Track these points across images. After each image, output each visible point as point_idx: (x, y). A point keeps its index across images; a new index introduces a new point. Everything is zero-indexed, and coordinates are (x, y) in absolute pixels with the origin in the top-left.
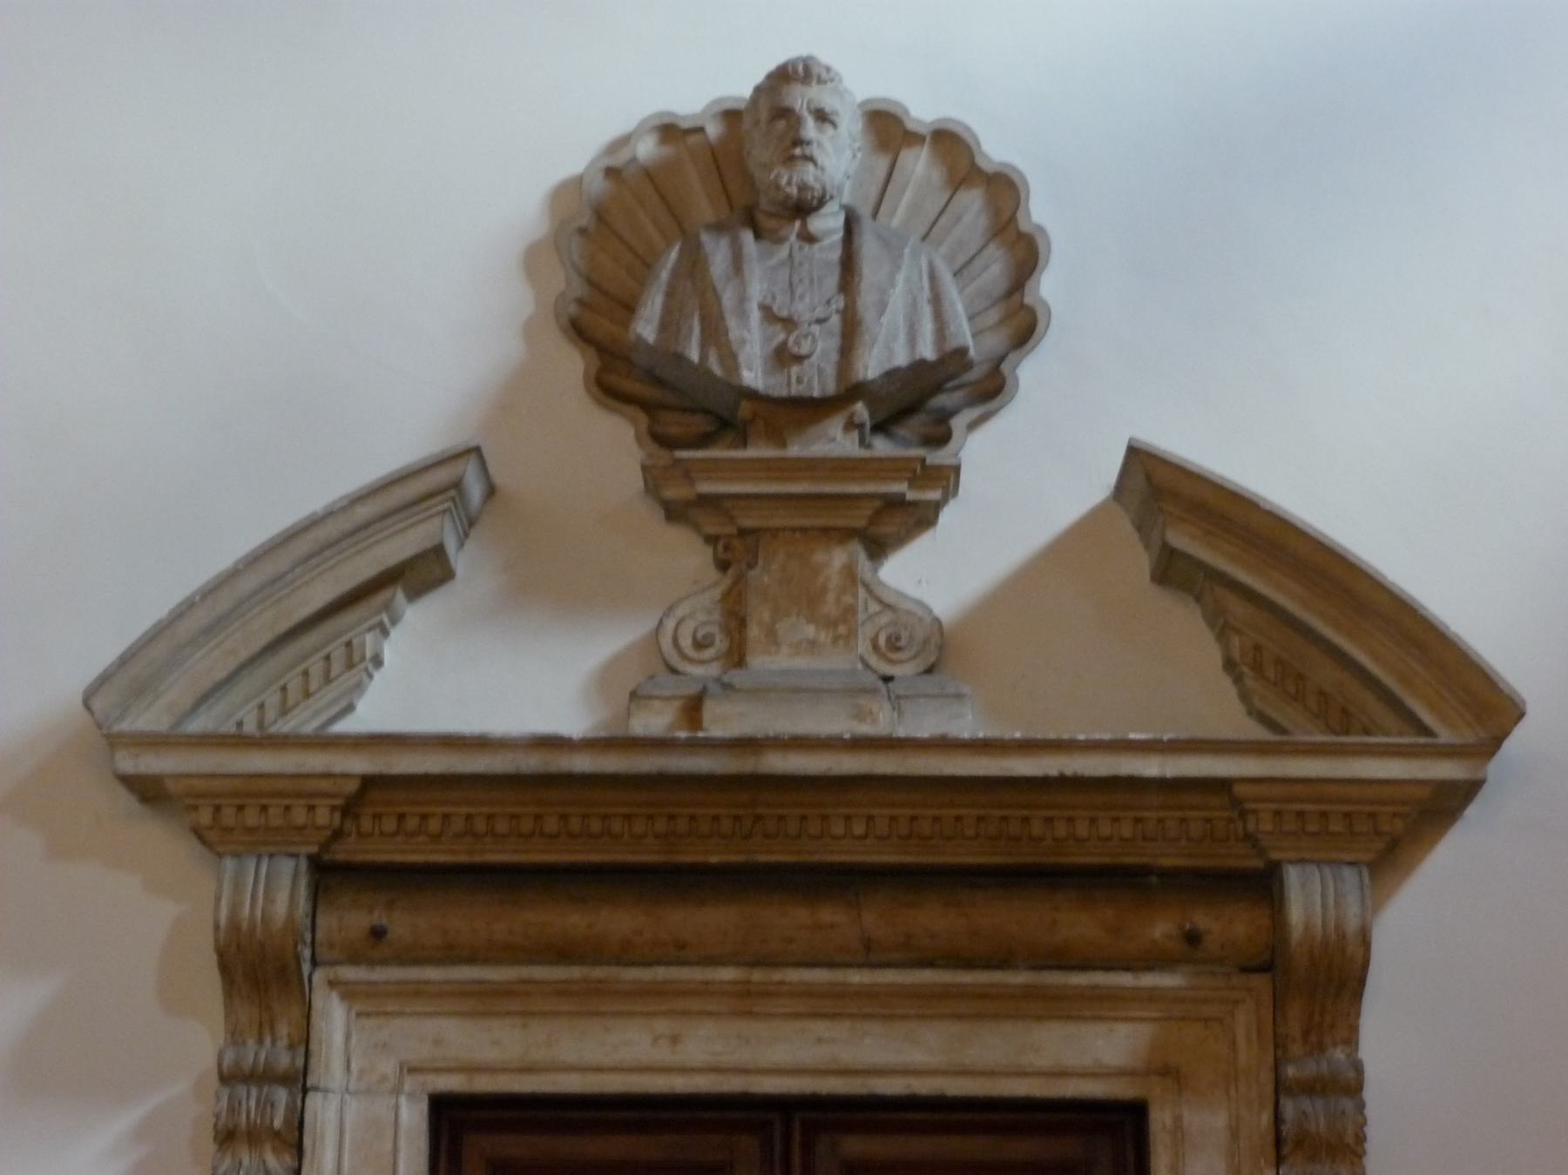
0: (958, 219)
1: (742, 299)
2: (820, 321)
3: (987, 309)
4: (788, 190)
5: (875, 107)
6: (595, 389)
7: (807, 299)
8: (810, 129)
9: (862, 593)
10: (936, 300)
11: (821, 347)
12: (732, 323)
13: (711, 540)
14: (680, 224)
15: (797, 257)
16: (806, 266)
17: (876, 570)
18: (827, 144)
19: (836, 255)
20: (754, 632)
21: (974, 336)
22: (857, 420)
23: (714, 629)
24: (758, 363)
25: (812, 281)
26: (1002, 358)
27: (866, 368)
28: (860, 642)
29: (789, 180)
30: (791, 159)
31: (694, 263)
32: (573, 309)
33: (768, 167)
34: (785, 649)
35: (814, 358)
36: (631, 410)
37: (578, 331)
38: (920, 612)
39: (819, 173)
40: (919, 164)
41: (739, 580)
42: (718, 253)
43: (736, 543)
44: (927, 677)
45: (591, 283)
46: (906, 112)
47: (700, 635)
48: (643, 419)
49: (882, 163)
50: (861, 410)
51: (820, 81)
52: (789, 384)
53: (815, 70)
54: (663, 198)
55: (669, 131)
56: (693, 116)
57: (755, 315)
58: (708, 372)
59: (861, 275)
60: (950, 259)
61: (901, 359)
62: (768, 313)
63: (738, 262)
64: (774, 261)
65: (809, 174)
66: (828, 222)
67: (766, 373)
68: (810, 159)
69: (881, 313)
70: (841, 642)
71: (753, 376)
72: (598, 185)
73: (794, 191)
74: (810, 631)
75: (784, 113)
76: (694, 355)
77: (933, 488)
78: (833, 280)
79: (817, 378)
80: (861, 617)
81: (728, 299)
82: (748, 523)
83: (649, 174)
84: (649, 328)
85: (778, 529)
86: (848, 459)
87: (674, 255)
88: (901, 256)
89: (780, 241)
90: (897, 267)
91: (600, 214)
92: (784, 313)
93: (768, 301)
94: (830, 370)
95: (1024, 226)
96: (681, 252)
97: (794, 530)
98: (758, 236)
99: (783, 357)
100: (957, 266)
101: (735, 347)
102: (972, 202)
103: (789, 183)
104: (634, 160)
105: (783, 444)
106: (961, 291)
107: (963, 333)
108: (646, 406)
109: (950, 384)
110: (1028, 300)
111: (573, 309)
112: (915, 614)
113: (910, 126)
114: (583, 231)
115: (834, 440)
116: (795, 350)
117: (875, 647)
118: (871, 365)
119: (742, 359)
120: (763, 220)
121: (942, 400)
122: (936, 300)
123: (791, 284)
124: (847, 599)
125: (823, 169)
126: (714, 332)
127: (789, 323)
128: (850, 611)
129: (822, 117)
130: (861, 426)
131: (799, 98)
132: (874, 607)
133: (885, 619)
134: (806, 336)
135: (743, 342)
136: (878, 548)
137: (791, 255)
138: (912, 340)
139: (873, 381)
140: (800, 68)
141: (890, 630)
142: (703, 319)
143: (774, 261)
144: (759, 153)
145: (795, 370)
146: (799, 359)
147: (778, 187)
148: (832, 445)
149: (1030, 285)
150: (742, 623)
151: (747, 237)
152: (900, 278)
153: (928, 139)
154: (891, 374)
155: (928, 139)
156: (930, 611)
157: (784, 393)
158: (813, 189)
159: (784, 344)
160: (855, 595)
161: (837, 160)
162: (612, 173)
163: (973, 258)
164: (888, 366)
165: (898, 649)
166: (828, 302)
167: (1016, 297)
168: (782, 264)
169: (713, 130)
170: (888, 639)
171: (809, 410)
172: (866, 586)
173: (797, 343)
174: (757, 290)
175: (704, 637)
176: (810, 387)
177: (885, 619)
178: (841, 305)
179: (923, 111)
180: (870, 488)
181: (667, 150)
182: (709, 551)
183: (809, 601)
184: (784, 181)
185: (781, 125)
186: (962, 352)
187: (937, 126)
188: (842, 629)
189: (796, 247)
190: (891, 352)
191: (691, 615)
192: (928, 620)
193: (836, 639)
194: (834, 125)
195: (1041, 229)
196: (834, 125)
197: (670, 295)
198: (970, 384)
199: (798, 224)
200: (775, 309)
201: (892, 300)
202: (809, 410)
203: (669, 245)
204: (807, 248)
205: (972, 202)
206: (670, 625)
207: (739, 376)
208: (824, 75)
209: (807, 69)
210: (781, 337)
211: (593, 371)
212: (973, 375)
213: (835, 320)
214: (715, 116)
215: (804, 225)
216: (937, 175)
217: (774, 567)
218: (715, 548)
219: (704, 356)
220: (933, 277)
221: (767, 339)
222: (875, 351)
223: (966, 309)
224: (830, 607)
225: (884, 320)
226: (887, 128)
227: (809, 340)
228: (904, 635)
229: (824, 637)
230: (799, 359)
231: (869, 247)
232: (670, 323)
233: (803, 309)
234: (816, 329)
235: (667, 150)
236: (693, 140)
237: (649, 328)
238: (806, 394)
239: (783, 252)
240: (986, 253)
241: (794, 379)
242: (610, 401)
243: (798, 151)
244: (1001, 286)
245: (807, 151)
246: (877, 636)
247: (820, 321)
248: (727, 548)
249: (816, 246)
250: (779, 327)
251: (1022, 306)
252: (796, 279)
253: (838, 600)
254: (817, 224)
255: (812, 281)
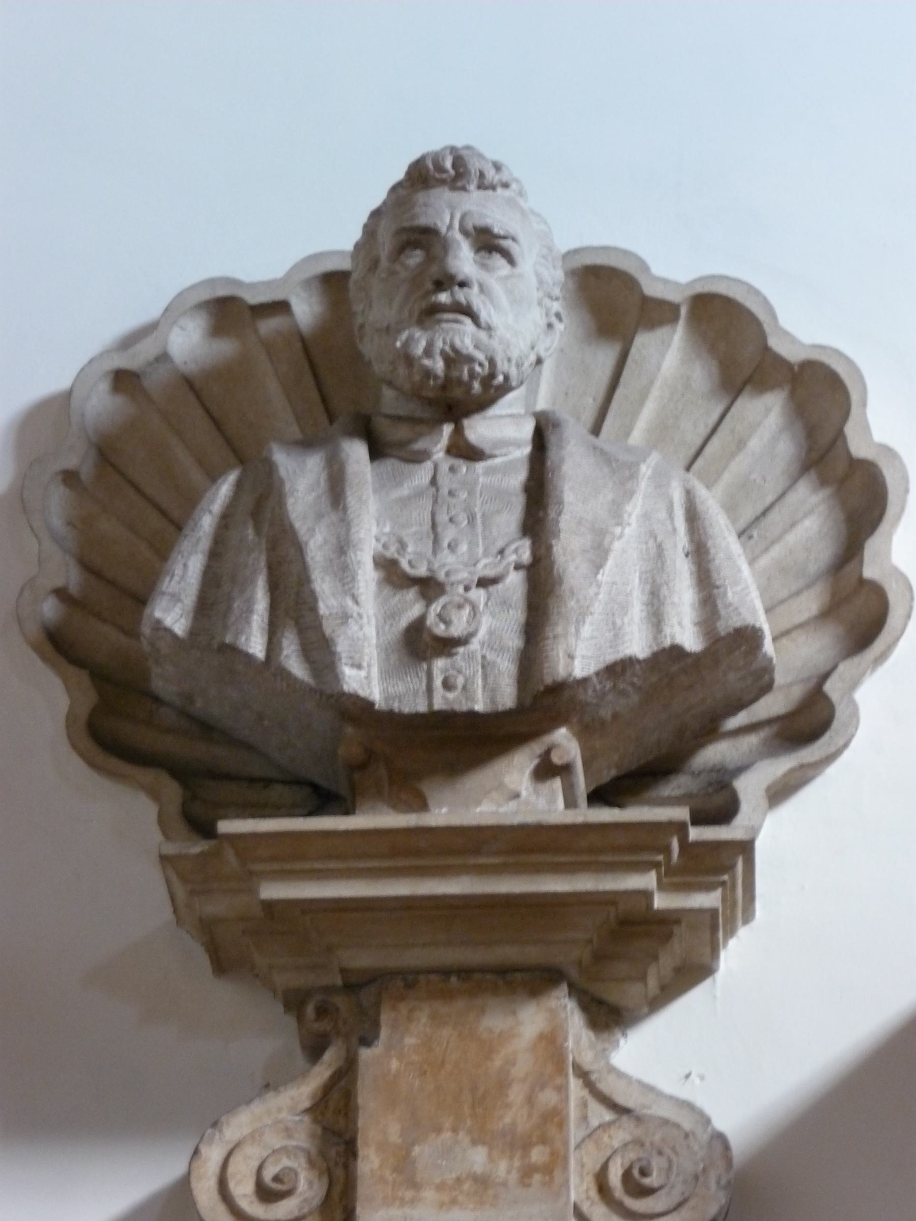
0: (741, 444)
1: (343, 547)
2: (484, 583)
3: (798, 593)
4: (427, 362)
5: (589, 260)
6: (87, 743)
7: (463, 548)
8: (464, 260)
9: (574, 1085)
10: (700, 553)
11: (490, 628)
12: (323, 585)
13: (294, 1002)
14: (234, 451)
15: (445, 481)
16: (463, 495)
17: (604, 1054)
18: (497, 288)
19: (518, 478)
20: (369, 1162)
21: (768, 611)
22: (556, 759)
23: (299, 1164)
24: (371, 654)
25: (472, 519)
26: (825, 676)
27: (571, 657)
28: (573, 1180)
29: (427, 346)
30: (430, 314)
31: (262, 501)
32: (50, 609)
33: (390, 331)
34: (429, 1194)
35: (475, 645)
36: (148, 775)
37: (59, 645)
38: (687, 1124)
39: (483, 335)
40: (668, 358)
41: (346, 1073)
42: (301, 479)
43: (340, 1002)
44: (687, 1072)
45: (86, 566)
46: (644, 266)
47: (269, 1174)
48: (173, 790)
49: (603, 358)
50: (565, 742)
51: (483, 185)
52: (430, 690)
53: (474, 165)
54: (217, 423)
55: (227, 311)
56: (269, 284)
57: (367, 577)
58: (284, 674)
59: (561, 503)
60: (731, 508)
61: (637, 644)
62: (392, 573)
63: (336, 488)
64: (405, 490)
65: (464, 336)
66: (503, 428)
67: (387, 674)
68: (468, 311)
69: (598, 566)
70: (537, 1178)
71: (367, 674)
72: (100, 403)
73: (438, 365)
74: (478, 1158)
75: (424, 239)
76: (256, 646)
77: (709, 888)
78: (509, 519)
79: (482, 680)
80: (575, 1133)
81: (317, 546)
82: (362, 959)
83: (191, 385)
84: (178, 610)
85: (418, 972)
86: (540, 829)
87: (225, 489)
88: (633, 476)
89: (419, 458)
90: (629, 495)
91: (107, 452)
92: (422, 571)
93: (392, 552)
94: (506, 668)
95: (858, 448)
96: (239, 485)
97: (446, 972)
98: (376, 453)
99: (420, 645)
100: (742, 523)
101: (328, 628)
102: (765, 418)
103: (428, 352)
104: (164, 357)
105: (422, 805)
106: (752, 562)
107: (748, 599)
108: (180, 772)
109: (733, 723)
110: (869, 572)
111: (50, 609)
112: (677, 1126)
113: (651, 290)
114: (70, 477)
115: (511, 793)
116: (440, 630)
117: (603, 1188)
118: (580, 653)
119: (342, 647)
120: (383, 426)
121: (715, 753)
122: (700, 553)
123: (434, 526)
124: (548, 1098)
125: (489, 329)
126: (293, 605)
127: (429, 587)
128: (555, 1118)
129: (488, 243)
130: (565, 770)
131: (444, 211)
132: (600, 1115)
133: (620, 1136)
134: (460, 607)
135: (345, 617)
136: (608, 1017)
137: (434, 482)
138: (656, 616)
139: (584, 682)
140: (448, 164)
141: (632, 1155)
142: (274, 588)
143: (405, 490)
144: (377, 310)
145: (440, 664)
146: (447, 646)
147: (409, 360)
148: (512, 805)
149: (872, 546)
150: (350, 1149)
151: (356, 452)
152: (635, 509)
153: (683, 311)
154: (617, 670)
155: (683, 311)
156: (707, 1121)
157: (421, 707)
158: (470, 359)
159: (421, 620)
160: (562, 1089)
161: (515, 318)
162: (123, 380)
163: (764, 513)
164: (611, 657)
165: (646, 1192)
166: (501, 552)
167: (850, 568)
168: (418, 494)
169: (306, 310)
170: (627, 1176)
171: (467, 741)
172: (583, 1075)
173: (443, 618)
174: (370, 532)
175: (277, 1179)
176: (471, 698)
177: (620, 1136)
178: (526, 556)
179: (673, 266)
180: (584, 883)
181: (225, 348)
182: (291, 1021)
183: (475, 1104)
184: (419, 349)
185: (415, 258)
186: (748, 637)
187: (699, 289)
188: (538, 1155)
189: (444, 467)
190: (617, 633)
191: (254, 1136)
192: (704, 1137)
193: (527, 1172)
194: (507, 255)
195: (888, 450)
196: (507, 255)
197: (215, 555)
198: (769, 722)
199: (447, 429)
200: (404, 564)
201: (617, 545)
202: (467, 741)
203: (214, 477)
204: (463, 467)
205: (765, 418)
206: (213, 1155)
207: (337, 678)
208: (491, 175)
209: (459, 162)
210: (415, 611)
211: (84, 712)
212: (770, 706)
213: (515, 581)
214: (307, 283)
215: (458, 431)
216: (701, 375)
217: (410, 1041)
218: (300, 1019)
219: (272, 645)
220: (693, 517)
221: (391, 616)
222: (587, 630)
223: (763, 592)
224: (515, 1114)
225: (604, 576)
226: (609, 299)
227: (467, 610)
228: (657, 1164)
229: (504, 1169)
230: (447, 646)
231: (574, 463)
232: (213, 601)
233: (455, 564)
234: (478, 595)
235: (225, 348)
236: (269, 326)
237: (178, 610)
238: (463, 706)
239: (422, 474)
240: (793, 498)
241: (438, 682)
242: (114, 763)
243: (444, 298)
244: (823, 553)
245: (461, 295)
246: (605, 1168)
247: (484, 583)
248: (322, 1012)
249: (480, 466)
250: (411, 594)
251: (862, 582)
252: (443, 518)
253: (530, 1101)
254: (479, 429)
255: (472, 519)
